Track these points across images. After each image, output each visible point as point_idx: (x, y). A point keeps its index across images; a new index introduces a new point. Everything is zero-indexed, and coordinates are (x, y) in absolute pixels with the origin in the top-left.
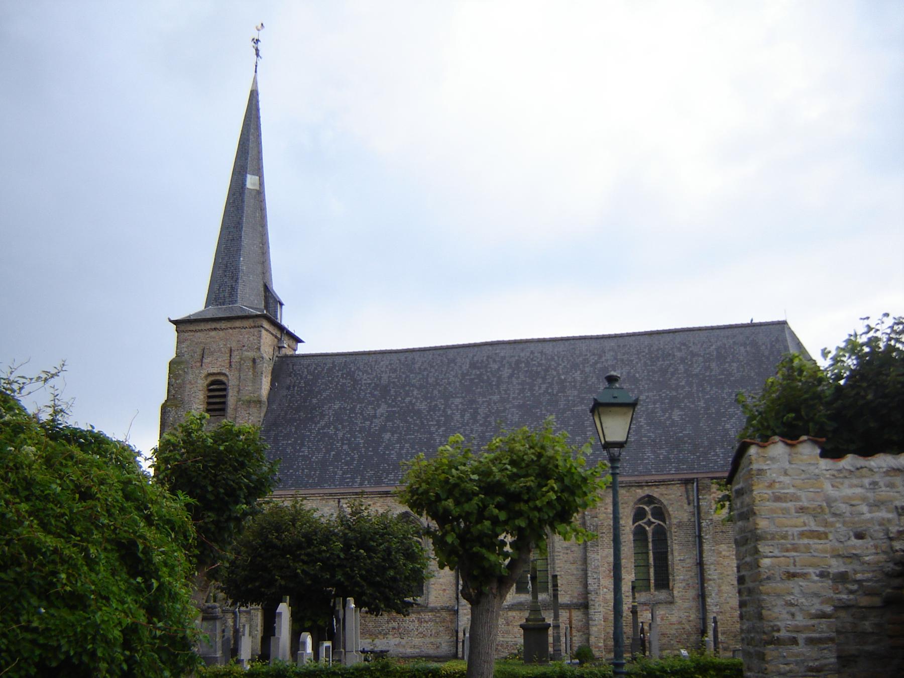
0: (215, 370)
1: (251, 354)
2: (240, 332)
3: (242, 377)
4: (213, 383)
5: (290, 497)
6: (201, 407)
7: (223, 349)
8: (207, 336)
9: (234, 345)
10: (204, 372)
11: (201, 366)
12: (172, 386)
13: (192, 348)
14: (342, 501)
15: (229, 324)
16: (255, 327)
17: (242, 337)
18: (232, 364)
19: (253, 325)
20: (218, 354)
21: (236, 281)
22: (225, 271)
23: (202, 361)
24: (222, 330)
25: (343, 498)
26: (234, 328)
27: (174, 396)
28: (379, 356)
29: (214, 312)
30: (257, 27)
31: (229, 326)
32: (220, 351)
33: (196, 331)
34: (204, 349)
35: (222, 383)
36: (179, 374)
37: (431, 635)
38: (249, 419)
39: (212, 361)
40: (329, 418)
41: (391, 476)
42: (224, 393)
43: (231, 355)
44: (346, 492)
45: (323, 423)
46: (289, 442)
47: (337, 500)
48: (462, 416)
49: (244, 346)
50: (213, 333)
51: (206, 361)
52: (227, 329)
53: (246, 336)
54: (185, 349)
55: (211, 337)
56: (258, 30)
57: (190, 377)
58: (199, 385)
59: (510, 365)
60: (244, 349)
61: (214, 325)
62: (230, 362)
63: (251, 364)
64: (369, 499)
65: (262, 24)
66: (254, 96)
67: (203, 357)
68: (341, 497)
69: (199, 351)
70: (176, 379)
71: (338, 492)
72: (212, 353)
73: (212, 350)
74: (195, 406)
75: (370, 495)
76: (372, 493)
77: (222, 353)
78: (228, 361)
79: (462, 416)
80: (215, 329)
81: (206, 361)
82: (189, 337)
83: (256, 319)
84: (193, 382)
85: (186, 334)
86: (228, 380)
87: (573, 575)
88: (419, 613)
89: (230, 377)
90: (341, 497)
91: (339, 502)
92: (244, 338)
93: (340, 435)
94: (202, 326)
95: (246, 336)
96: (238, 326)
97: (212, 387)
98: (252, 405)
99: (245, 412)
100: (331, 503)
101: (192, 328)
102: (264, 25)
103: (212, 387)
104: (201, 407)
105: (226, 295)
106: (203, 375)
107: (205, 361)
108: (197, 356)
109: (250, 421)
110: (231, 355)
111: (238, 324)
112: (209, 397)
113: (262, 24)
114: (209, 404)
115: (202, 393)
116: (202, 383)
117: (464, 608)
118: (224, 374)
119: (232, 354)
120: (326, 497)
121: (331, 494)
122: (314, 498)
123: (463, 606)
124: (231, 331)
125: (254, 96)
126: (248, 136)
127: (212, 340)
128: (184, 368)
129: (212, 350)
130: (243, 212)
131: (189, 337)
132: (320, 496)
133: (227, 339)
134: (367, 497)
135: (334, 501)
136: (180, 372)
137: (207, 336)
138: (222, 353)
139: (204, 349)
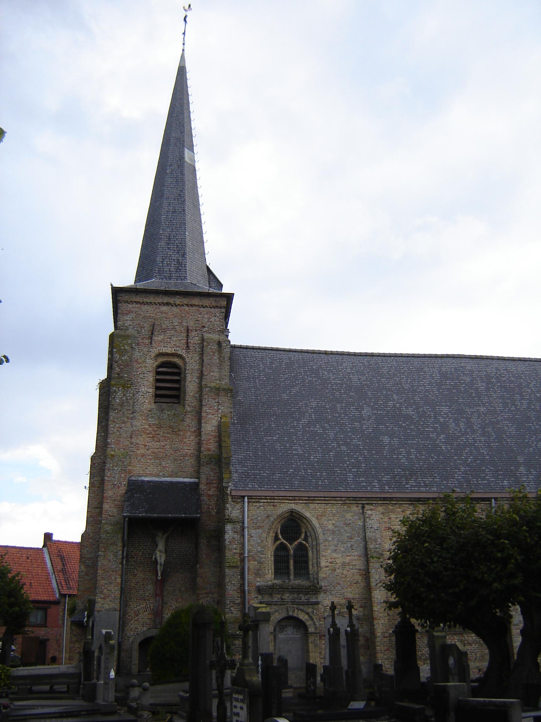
0: (169, 350)
1: (215, 337)
2: (199, 310)
3: (205, 361)
4: (162, 365)
5: (305, 500)
6: (151, 390)
7: (177, 327)
8: (158, 310)
9: (191, 324)
10: (155, 351)
11: (151, 343)
12: (116, 362)
13: (138, 322)
14: (367, 507)
15: (185, 301)
16: (217, 307)
17: (201, 316)
18: (190, 345)
19: (214, 304)
20: (173, 332)
21: (184, 255)
22: (169, 244)
23: (151, 338)
24: (176, 306)
25: (368, 504)
26: (192, 306)
27: (118, 374)
28: (340, 357)
29: (141, 285)
30: (184, 8)
31: (185, 302)
32: (174, 328)
33: (143, 303)
34: (154, 325)
35: (175, 365)
36: (125, 349)
37: (475, 659)
38: (218, 409)
39: (164, 339)
40: (310, 416)
41: (412, 482)
42: (158, 377)
43: (188, 335)
44: (372, 496)
45: (304, 421)
46: (274, 438)
47: (360, 506)
48: (457, 425)
49: (204, 327)
50: (164, 308)
51: (156, 338)
52: (183, 305)
53: (206, 316)
54: (129, 323)
55: (162, 312)
56: (186, 10)
57: (137, 354)
58: (147, 365)
59: (481, 378)
60: (205, 329)
61: (166, 299)
62: (187, 343)
63: (216, 347)
64: (397, 506)
65: (189, 6)
66: (182, 72)
67: (152, 333)
68: (365, 502)
69: (147, 327)
70: (122, 355)
71: (363, 496)
72: (164, 331)
73: (164, 326)
74: (143, 389)
75: (399, 501)
76: (402, 499)
77: (176, 331)
78: (185, 341)
79: (457, 425)
80: (168, 304)
81: (156, 338)
82: (134, 310)
83: (218, 299)
84: (140, 361)
85: (130, 306)
86: (185, 363)
87: (123, 623)
88: (461, 634)
89: (187, 360)
90: (365, 502)
91: (363, 507)
92: (202, 318)
93: (332, 435)
94: (151, 299)
95: (206, 316)
96: (196, 303)
97: (160, 369)
98: (222, 393)
99: (213, 401)
100: (354, 508)
101: (139, 299)
102: (191, 7)
103: (160, 369)
104: (151, 390)
105: (172, 269)
106: (153, 355)
107: (155, 338)
108: (145, 332)
109: (220, 411)
110: (188, 335)
111: (196, 301)
112: (157, 381)
113: (189, 6)
114: (157, 388)
115: (151, 374)
116: (151, 364)
117: (516, 627)
118: (180, 356)
119: (190, 335)
120: (348, 502)
121: (355, 499)
122: (333, 502)
123: (515, 625)
124: (186, 308)
125: (182, 72)
126: (182, 110)
127: (164, 315)
128: (131, 343)
129: (164, 326)
130: (184, 184)
131: (134, 310)
132: (341, 500)
133: (182, 317)
134: (395, 504)
135: (357, 507)
136: (126, 347)
137: (158, 310)
138: (176, 331)
139: (154, 325)
